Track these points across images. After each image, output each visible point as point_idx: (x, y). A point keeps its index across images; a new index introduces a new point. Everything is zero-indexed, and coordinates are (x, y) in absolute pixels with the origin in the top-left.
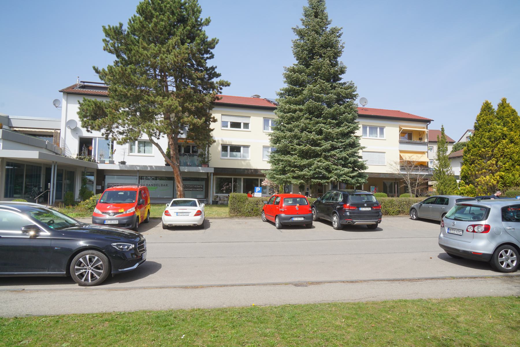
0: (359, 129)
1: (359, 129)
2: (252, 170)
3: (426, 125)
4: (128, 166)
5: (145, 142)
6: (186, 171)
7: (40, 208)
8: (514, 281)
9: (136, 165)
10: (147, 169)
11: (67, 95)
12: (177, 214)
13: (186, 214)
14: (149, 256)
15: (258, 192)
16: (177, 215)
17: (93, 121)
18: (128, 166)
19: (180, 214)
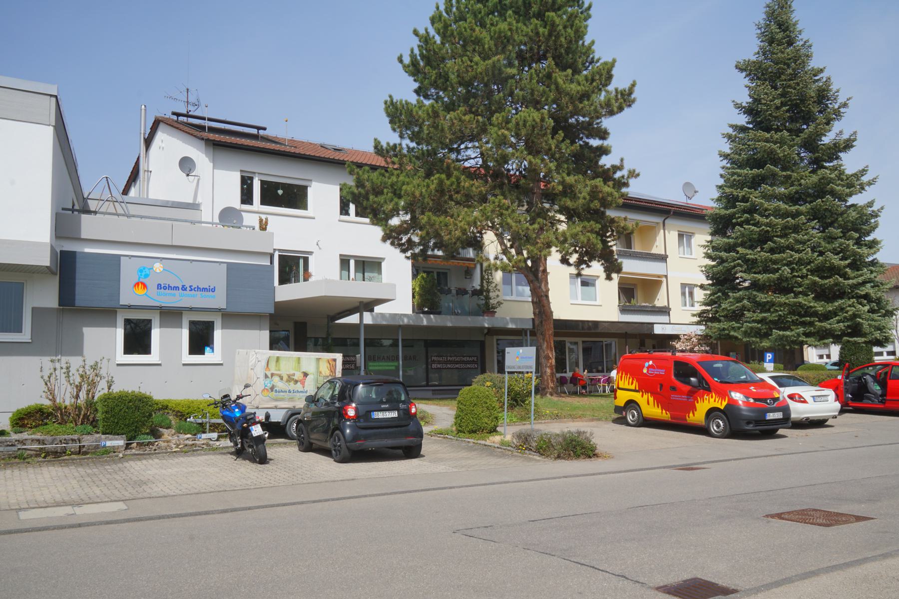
0: (854, 144)
1: (854, 144)
2: (590, 324)
3: (663, 220)
4: (388, 315)
5: (364, 261)
6: (486, 325)
7: (665, 351)
8: (35, 453)
9: (402, 314)
10: (423, 323)
11: (214, 148)
12: (814, 399)
13: (823, 399)
14: (269, 456)
15: (770, 361)
16: (815, 401)
17: (446, 114)
18: (388, 315)
19: (819, 399)
